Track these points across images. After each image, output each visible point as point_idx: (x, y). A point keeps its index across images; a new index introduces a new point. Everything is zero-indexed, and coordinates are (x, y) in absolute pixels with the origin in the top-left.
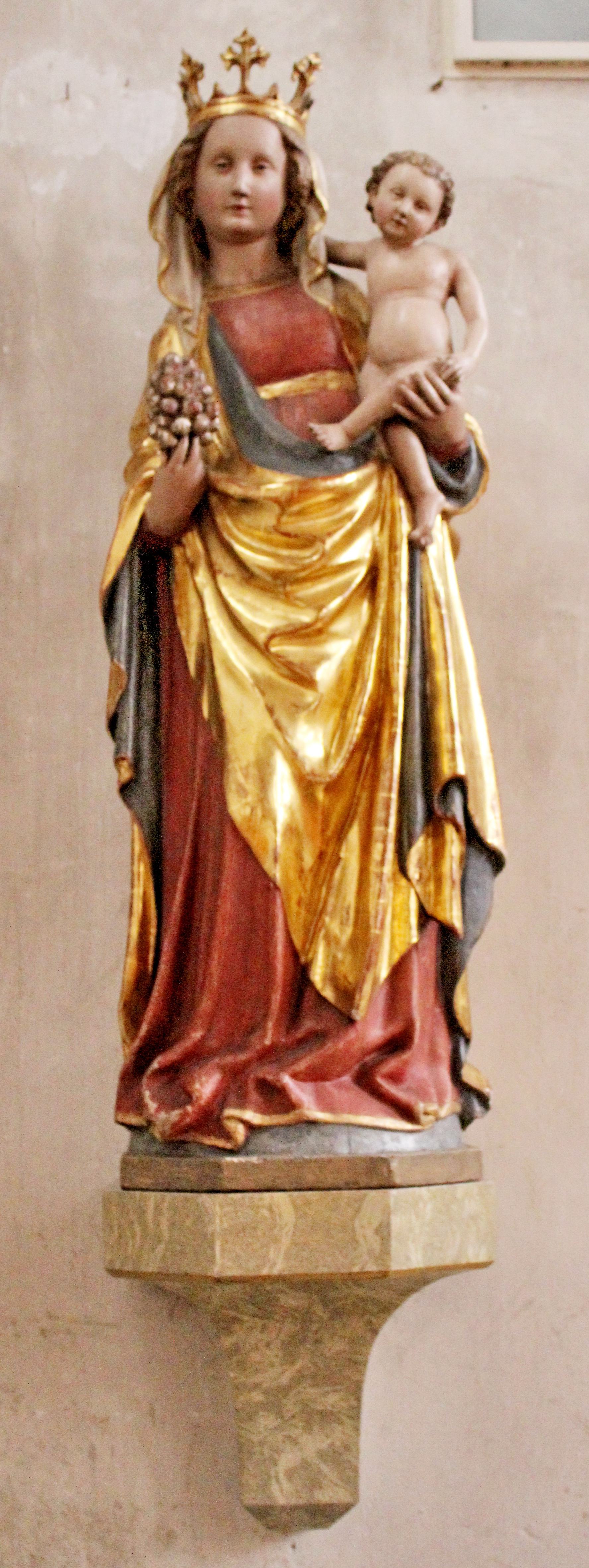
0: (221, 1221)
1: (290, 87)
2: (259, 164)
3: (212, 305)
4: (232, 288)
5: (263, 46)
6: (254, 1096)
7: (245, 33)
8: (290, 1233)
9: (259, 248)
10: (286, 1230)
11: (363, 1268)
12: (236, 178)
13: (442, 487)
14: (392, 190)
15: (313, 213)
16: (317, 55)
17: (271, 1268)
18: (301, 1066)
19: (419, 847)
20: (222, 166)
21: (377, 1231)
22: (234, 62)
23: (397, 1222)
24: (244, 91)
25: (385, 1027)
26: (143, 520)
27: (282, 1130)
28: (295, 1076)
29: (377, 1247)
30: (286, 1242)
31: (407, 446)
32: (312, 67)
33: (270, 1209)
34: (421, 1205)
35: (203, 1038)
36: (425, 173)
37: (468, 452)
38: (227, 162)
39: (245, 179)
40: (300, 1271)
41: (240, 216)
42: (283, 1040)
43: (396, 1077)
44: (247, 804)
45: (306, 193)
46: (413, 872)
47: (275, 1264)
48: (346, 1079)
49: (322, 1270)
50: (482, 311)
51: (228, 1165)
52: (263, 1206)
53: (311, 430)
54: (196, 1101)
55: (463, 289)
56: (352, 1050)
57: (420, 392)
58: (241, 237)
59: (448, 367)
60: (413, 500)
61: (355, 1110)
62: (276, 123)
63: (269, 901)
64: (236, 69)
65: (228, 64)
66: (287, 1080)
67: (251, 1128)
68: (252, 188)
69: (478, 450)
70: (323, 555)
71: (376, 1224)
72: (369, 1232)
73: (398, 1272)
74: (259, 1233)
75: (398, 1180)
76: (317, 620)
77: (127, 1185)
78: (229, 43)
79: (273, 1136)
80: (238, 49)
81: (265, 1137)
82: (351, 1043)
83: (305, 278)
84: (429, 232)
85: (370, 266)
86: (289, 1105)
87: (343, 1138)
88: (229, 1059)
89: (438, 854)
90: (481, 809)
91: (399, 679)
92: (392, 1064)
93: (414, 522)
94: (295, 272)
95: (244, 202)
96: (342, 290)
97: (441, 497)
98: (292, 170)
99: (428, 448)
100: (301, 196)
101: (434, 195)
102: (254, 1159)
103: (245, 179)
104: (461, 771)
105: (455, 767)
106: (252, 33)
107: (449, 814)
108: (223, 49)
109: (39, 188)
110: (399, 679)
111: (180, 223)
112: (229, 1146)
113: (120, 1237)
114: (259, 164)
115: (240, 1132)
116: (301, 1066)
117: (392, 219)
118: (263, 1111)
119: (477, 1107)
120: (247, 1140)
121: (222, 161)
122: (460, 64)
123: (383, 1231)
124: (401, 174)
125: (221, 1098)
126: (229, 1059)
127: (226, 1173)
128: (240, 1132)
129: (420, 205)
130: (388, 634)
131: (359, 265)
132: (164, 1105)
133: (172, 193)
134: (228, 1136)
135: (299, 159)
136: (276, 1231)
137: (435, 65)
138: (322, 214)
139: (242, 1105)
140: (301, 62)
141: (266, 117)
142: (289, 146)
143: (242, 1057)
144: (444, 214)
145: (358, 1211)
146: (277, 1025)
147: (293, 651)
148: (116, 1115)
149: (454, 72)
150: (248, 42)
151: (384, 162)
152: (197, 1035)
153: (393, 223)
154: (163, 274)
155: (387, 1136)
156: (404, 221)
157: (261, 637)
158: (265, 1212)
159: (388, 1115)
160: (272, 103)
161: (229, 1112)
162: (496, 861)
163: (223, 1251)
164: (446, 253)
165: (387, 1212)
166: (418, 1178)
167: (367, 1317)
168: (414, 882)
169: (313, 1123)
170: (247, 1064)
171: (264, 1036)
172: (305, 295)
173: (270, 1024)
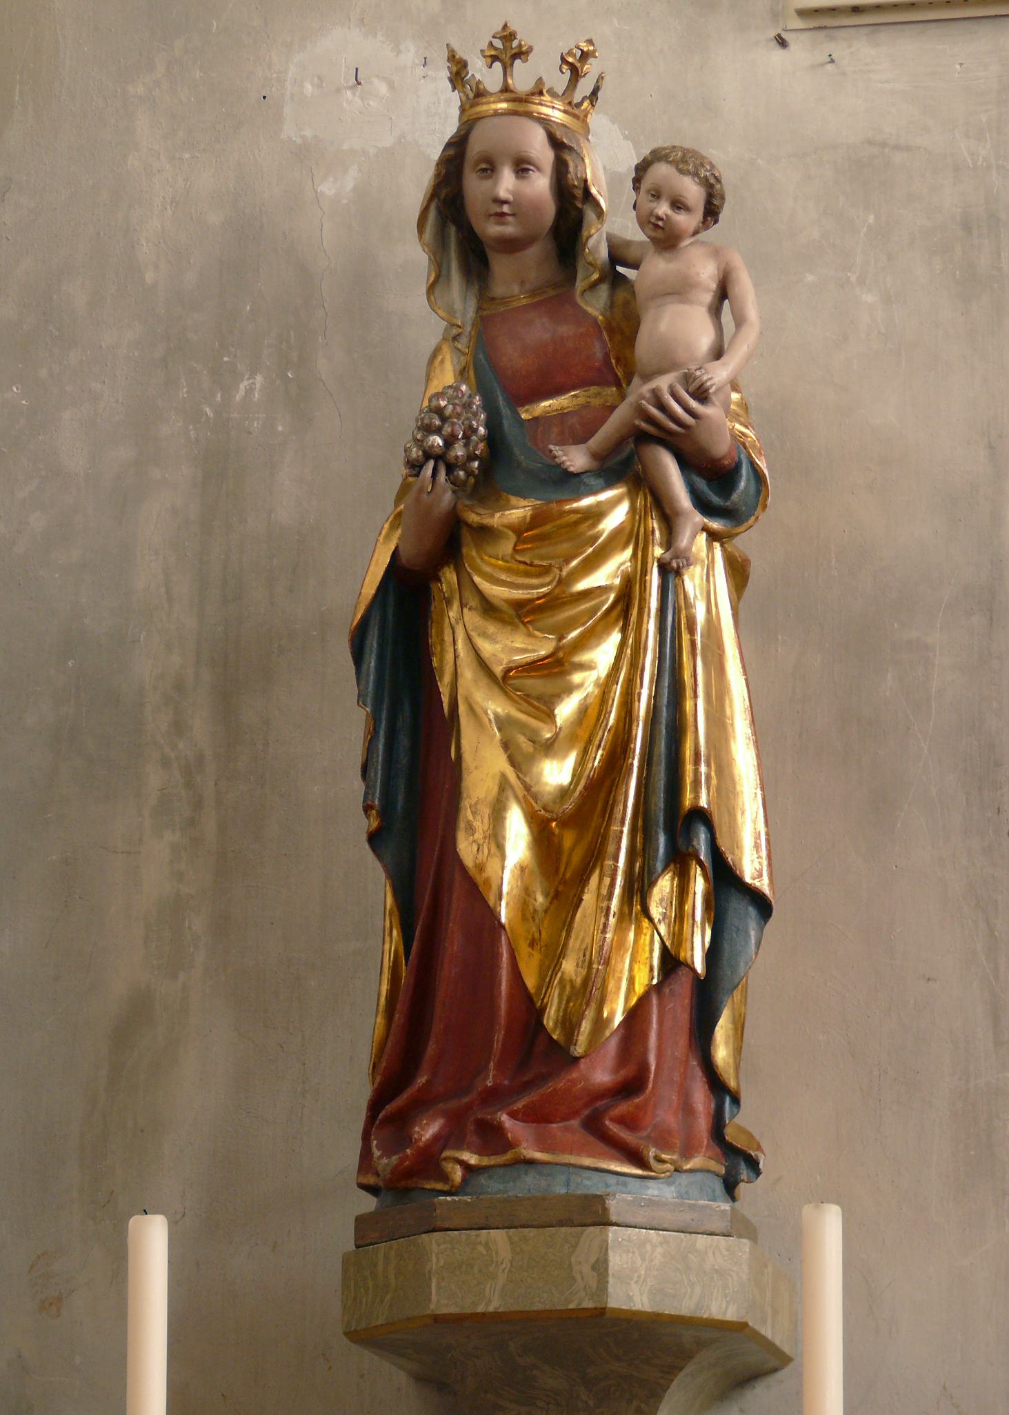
0: (438, 1259)
1: (559, 81)
2: (522, 167)
3: (482, 319)
4: (504, 300)
5: (524, 38)
6: (473, 1138)
7: (505, 26)
8: (506, 1271)
9: (533, 253)
10: (504, 1266)
11: (579, 1304)
12: (495, 184)
13: (704, 507)
14: (648, 191)
15: (590, 215)
16: (590, 42)
17: (487, 1305)
18: (519, 1105)
19: (665, 885)
20: (484, 170)
21: (593, 1268)
22: (495, 58)
23: (616, 1260)
24: (506, 89)
25: (616, 1070)
26: (395, 555)
27: (501, 1171)
28: (513, 1115)
29: (593, 1284)
30: (502, 1279)
31: (659, 465)
32: (585, 56)
33: (487, 1245)
34: (648, 1247)
35: (428, 1082)
36: (681, 172)
37: (737, 467)
38: (489, 168)
39: (507, 183)
40: (516, 1308)
41: (503, 224)
42: (506, 1082)
43: (630, 1123)
44: (474, 841)
45: (579, 193)
46: (656, 911)
47: (490, 1301)
48: (575, 1123)
49: (538, 1306)
50: (752, 313)
51: (441, 1203)
52: (480, 1243)
53: (551, 451)
54: (416, 1142)
55: (734, 290)
56: (574, 1090)
57: (662, 407)
58: (511, 246)
59: (695, 379)
60: (669, 521)
61: (581, 1150)
62: (544, 122)
63: (495, 941)
64: (498, 66)
65: (489, 60)
66: (504, 1118)
67: (467, 1167)
68: (514, 193)
69: (752, 464)
70: (560, 581)
71: (593, 1259)
72: (586, 1269)
73: (609, 1308)
74: (476, 1270)
75: (614, 1218)
76: (557, 649)
77: (360, 1242)
78: (488, 38)
79: (490, 1177)
80: (498, 44)
81: (482, 1180)
82: (573, 1082)
83: (580, 285)
84: (696, 233)
85: (642, 268)
86: (508, 1145)
87: (561, 1178)
88: (453, 1104)
89: (683, 891)
90: (736, 844)
91: (642, 707)
92: (623, 1108)
93: (668, 543)
94: (572, 278)
95: (506, 209)
96: (621, 295)
97: (699, 518)
98: (560, 168)
99: (685, 464)
100: (574, 197)
101: (693, 191)
102: (468, 1199)
103: (507, 183)
104: (703, 802)
105: (697, 797)
106: (513, 26)
107: (690, 850)
108: (485, 46)
109: (327, 188)
110: (642, 707)
111: (452, 230)
112: (446, 1188)
113: (355, 1298)
114: (522, 167)
115: (458, 1174)
116: (519, 1105)
117: (650, 222)
118: (480, 1153)
119: (744, 1173)
120: (464, 1180)
121: (484, 166)
122: (803, 13)
123: (601, 1267)
124: (661, 171)
125: (442, 1141)
126: (453, 1104)
127: (438, 1212)
128: (458, 1174)
129: (678, 204)
130: (636, 666)
131: (636, 266)
132: (387, 1153)
133: (439, 199)
134: (445, 1178)
135: (568, 158)
136: (491, 1269)
137: (775, 15)
138: (600, 213)
139: (459, 1147)
140: (570, 53)
141: (528, 115)
142: (557, 144)
143: (465, 1100)
144: (711, 212)
145: (575, 1247)
146: (499, 1066)
147: (534, 684)
148: (357, 1178)
149: (798, 23)
150: (508, 36)
151: (644, 160)
152: (422, 1080)
153: (651, 226)
154: (431, 289)
155: (612, 1180)
156: (660, 223)
157: (498, 670)
158: (481, 1249)
159: (618, 1159)
160: (536, 99)
161: (446, 1153)
162: (763, 906)
163: (439, 1287)
164: (716, 253)
165: (604, 1249)
166: (639, 1220)
167: (635, 1403)
168: (656, 921)
169: (531, 1162)
170: (469, 1107)
171: (486, 1079)
172: (576, 305)
173: (492, 1065)
